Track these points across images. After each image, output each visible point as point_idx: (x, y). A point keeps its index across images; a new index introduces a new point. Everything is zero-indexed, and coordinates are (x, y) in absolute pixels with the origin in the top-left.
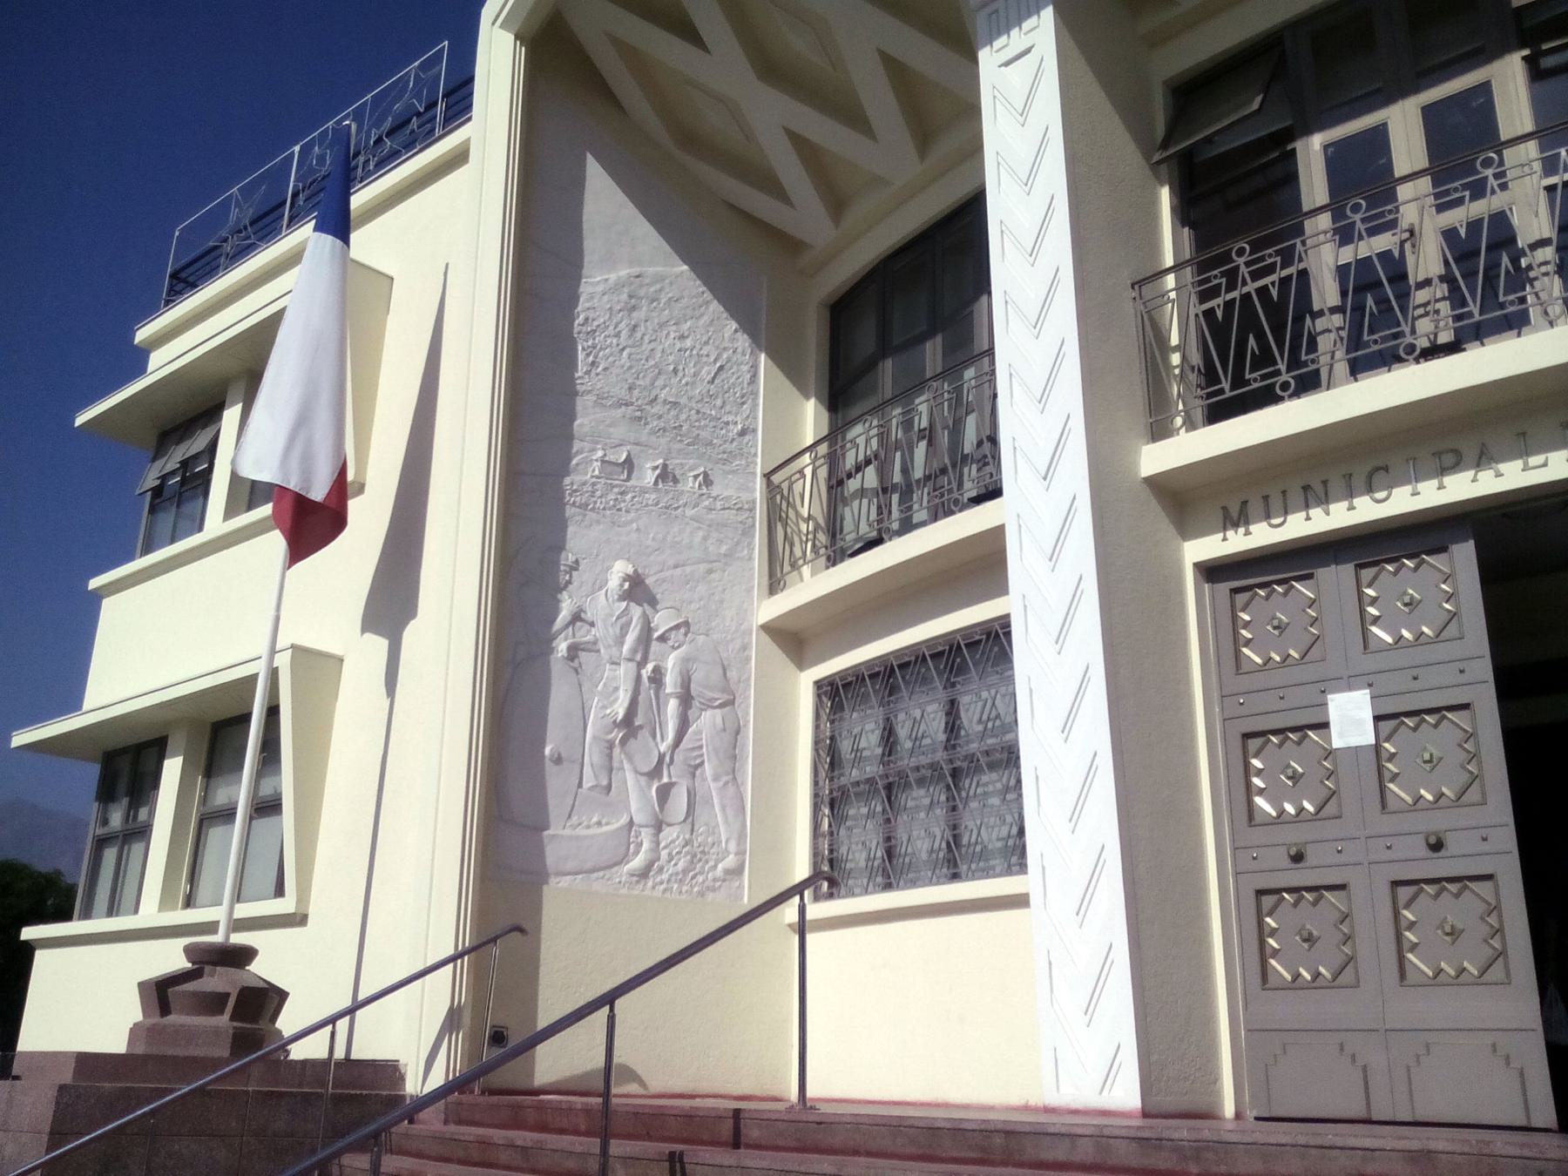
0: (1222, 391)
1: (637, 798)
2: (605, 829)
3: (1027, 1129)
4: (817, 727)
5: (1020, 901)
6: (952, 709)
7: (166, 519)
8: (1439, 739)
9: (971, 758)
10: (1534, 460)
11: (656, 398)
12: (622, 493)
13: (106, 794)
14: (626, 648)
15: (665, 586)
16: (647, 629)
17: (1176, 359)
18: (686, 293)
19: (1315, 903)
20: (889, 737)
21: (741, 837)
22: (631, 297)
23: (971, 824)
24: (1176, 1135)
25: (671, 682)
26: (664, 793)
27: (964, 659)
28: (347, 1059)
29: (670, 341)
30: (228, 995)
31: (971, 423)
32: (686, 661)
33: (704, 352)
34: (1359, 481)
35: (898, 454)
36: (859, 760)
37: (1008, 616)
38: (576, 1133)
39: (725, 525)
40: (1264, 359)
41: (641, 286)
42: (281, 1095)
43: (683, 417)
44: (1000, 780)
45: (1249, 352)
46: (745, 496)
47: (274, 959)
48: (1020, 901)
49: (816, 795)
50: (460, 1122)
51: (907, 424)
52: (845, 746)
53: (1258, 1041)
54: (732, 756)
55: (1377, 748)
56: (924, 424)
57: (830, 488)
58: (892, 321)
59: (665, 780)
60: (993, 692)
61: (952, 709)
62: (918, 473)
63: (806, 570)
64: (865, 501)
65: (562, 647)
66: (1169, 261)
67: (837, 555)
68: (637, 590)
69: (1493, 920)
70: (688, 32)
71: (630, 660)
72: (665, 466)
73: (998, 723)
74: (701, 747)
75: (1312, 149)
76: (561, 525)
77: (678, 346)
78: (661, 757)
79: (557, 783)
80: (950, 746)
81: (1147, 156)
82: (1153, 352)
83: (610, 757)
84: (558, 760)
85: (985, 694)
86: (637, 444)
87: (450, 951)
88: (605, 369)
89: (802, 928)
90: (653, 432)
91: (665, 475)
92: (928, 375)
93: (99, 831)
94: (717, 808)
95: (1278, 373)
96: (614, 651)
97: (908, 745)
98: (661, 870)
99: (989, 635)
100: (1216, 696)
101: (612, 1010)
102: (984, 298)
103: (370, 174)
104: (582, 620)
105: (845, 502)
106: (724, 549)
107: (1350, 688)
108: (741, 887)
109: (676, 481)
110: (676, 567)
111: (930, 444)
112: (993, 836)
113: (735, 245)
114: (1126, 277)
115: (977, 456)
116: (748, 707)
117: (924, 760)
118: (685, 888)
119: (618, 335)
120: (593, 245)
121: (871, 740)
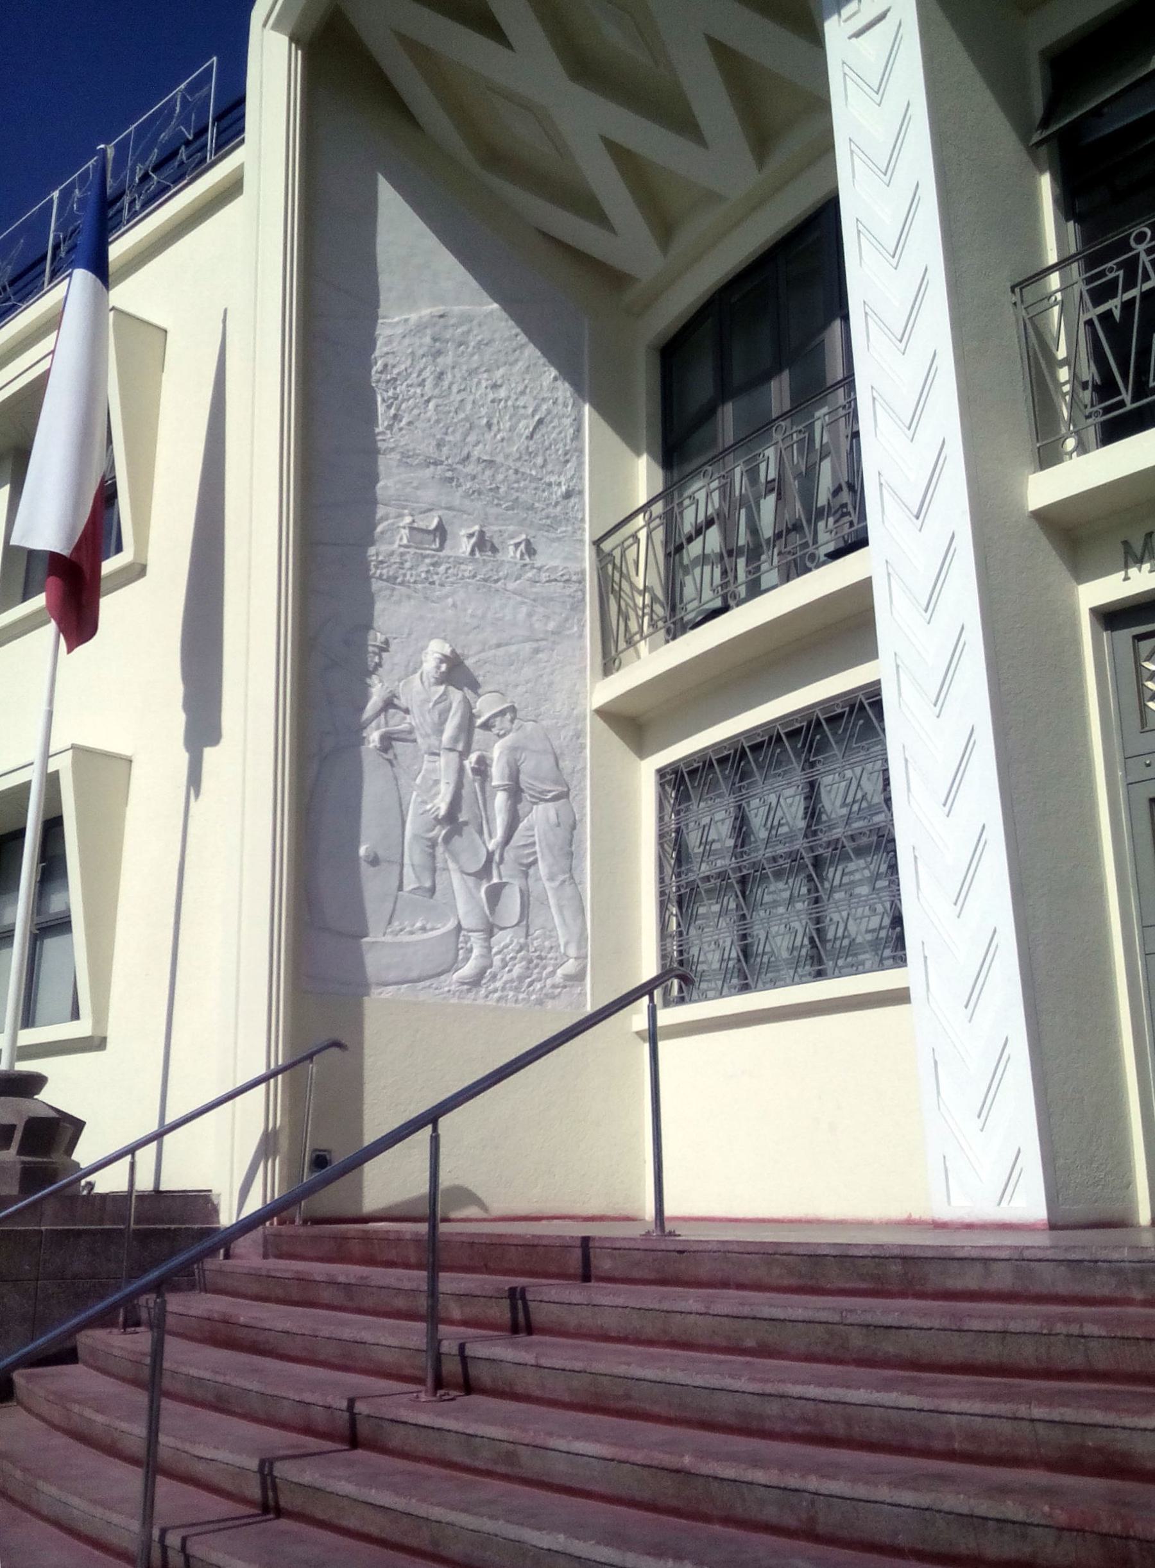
0: (1122, 404)
1: (464, 900)
3: (930, 1254)
4: (661, 819)
5: (900, 997)
6: (812, 791)
9: (835, 844)
11: (468, 456)
12: (434, 564)
15: (488, 667)
16: (469, 717)
17: (1064, 374)
18: (497, 336)
20: (742, 828)
22: (435, 340)
23: (836, 917)
24: (1115, 1256)
25: (497, 774)
26: (495, 894)
27: (825, 736)
28: (157, 1192)
29: (482, 390)
30: (13, 1127)
32: (514, 749)
33: (520, 403)
35: (743, 511)
36: (708, 853)
37: (878, 682)
38: (407, 1266)
39: (552, 599)
41: (446, 327)
42: (79, 1234)
43: (500, 477)
44: (867, 867)
46: (573, 567)
47: (64, 1087)
48: (900, 997)
49: (662, 893)
50: (280, 1256)
51: (752, 474)
52: (693, 839)
54: (568, 852)
56: (772, 475)
57: (668, 555)
58: (733, 358)
59: (495, 880)
60: (858, 770)
61: (812, 791)
62: (767, 531)
63: (643, 647)
64: (707, 569)
66: (1052, 258)
67: (677, 628)
68: (455, 672)
70: (490, 27)
71: (451, 750)
72: (482, 533)
73: (864, 804)
74: (533, 844)
76: (368, 602)
77: (491, 396)
78: (490, 855)
79: (374, 887)
80: (810, 832)
81: (1024, 137)
82: (1036, 358)
83: (433, 856)
84: (375, 861)
85: (849, 774)
86: (449, 508)
87: (261, 1070)
88: (410, 423)
89: (653, 1036)
90: (467, 495)
91: (483, 543)
92: (774, 416)
94: (554, 910)
96: (433, 741)
97: (763, 834)
98: (494, 977)
99: (852, 707)
100: (1118, 757)
101: (435, 1129)
102: (837, 324)
103: (136, 214)
104: (396, 707)
105: (687, 570)
106: (551, 626)
108: (583, 994)
109: (494, 550)
110: (499, 646)
113: (552, 280)
114: (1004, 279)
115: (836, 504)
116: (584, 799)
117: (781, 850)
118: (521, 996)
119: (422, 384)
120: (388, 280)
121: (722, 832)
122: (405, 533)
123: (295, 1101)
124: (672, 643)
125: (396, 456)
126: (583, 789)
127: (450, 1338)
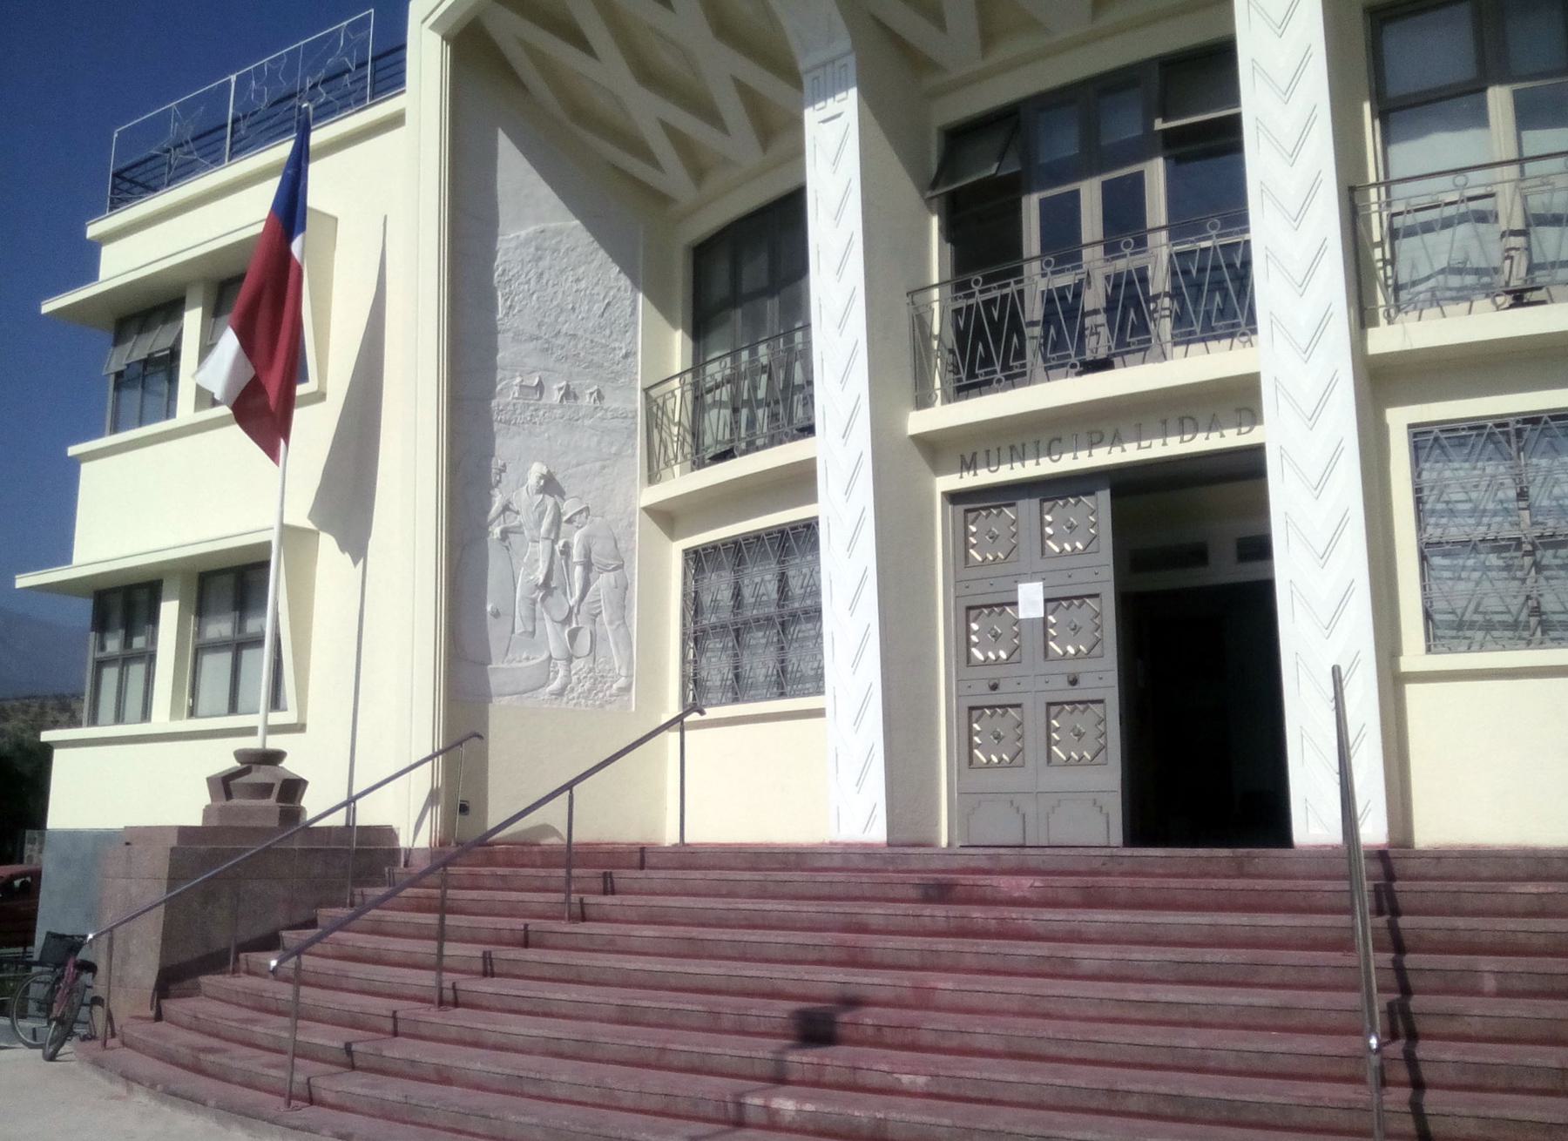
1: (553, 639)
2: (532, 662)
4: (685, 584)
5: (819, 713)
6: (783, 579)
7: (132, 397)
8: (1081, 614)
10: (1144, 444)
13: (101, 624)
14: (543, 530)
16: (558, 515)
17: (935, 344)
19: (1003, 715)
20: (737, 594)
21: (630, 662)
22: (537, 249)
26: (573, 635)
31: (798, 366)
34: (1043, 446)
36: (716, 608)
38: (533, 866)
40: (987, 361)
43: (581, 345)
45: (985, 350)
46: (630, 407)
48: (819, 713)
49: (684, 634)
52: (706, 599)
53: (965, 801)
54: (622, 606)
55: (1045, 619)
58: (739, 274)
61: (783, 579)
63: (677, 468)
65: (496, 531)
66: (935, 279)
68: (550, 485)
69: (1101, 727)
70: (579, 40)
72: (568, 386)
75: (1031, 205)
76: (489, 438)
78: (571, 609)
79: (496, 632)
81: (922, 193)
84: (496, 614)
87: (430, 753)
90: (558, 360)
91: (569, 394)
93: (99, 655)
95: (995, 372)
98: (572, 690)
106: (614, 450)
107: (1032, 580)
108: (629, 700)
109: (576, 397)
110: (578, 465)
111: (770, 377)
112: (808, 669)
113: (612, 193)
119: (528, 282)
120: (505, 210)
121: (725, 595)
122: (516, 389)
123: (450, 772)
124: (696, 472)
125: (511, 334)
126: (632, 562)
127: (575, 898)
